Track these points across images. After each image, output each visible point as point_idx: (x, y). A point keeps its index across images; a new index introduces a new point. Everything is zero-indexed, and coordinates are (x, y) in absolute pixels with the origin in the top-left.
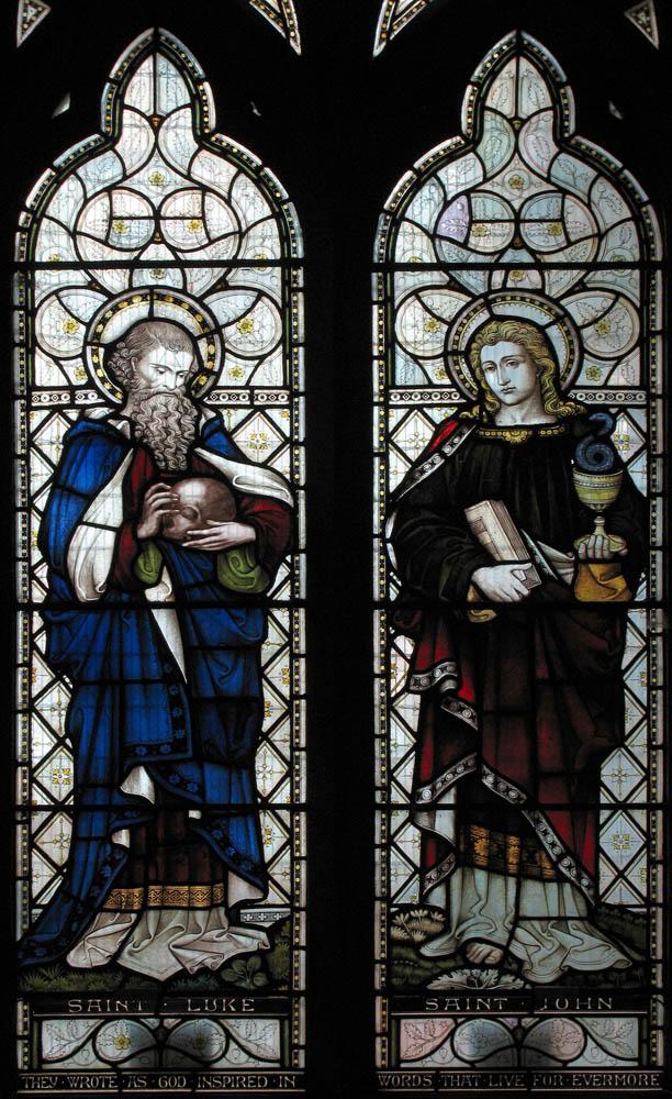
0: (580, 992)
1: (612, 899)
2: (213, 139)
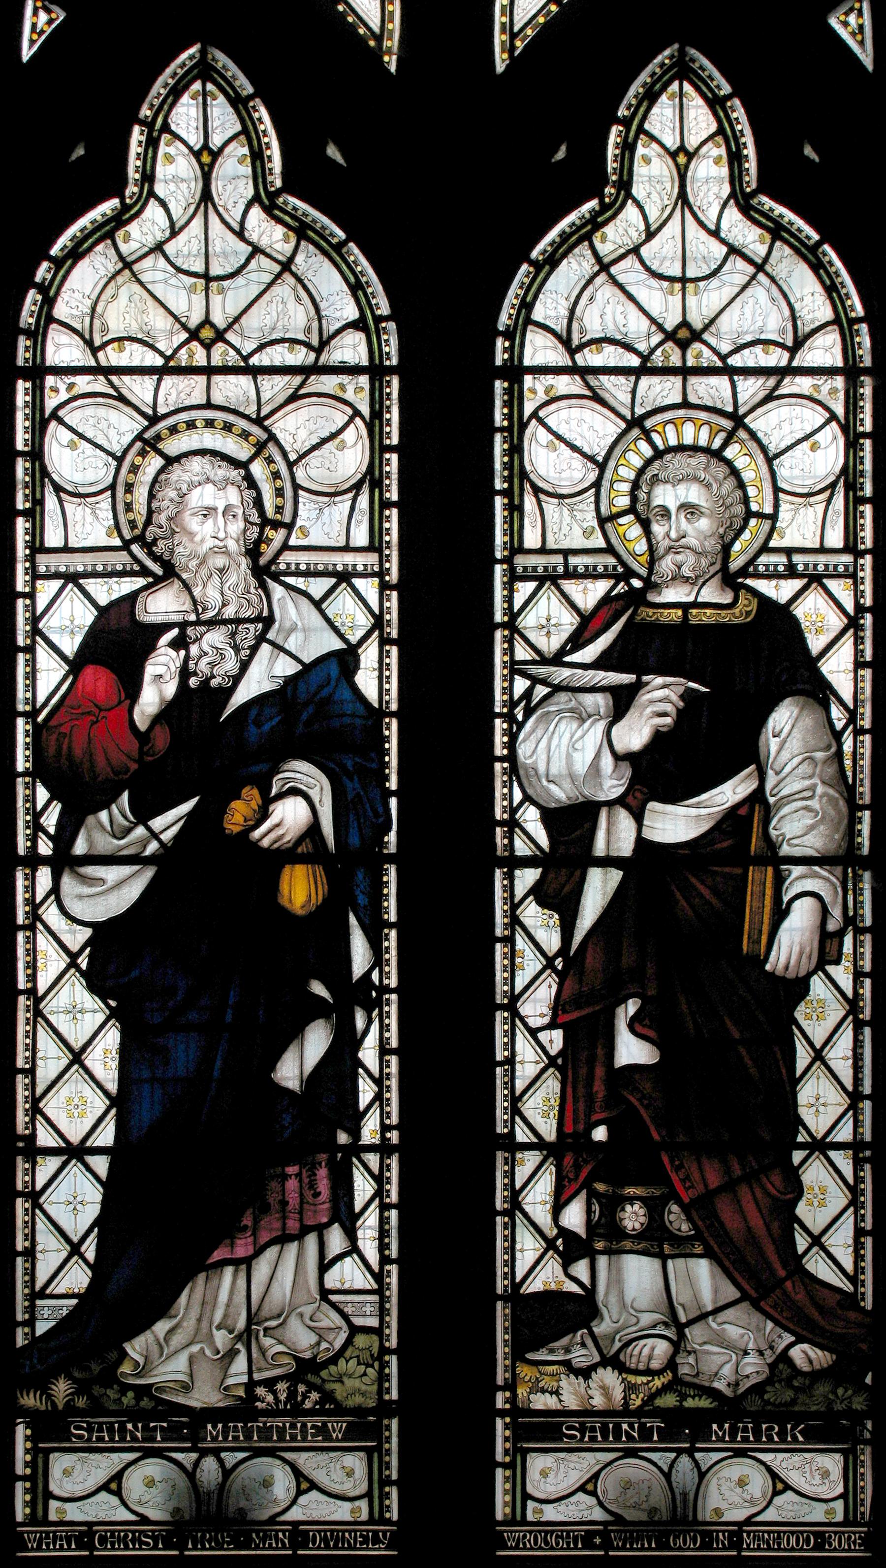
0: (759, 1415)
1: (536, 1285)
2: (128, 201)
